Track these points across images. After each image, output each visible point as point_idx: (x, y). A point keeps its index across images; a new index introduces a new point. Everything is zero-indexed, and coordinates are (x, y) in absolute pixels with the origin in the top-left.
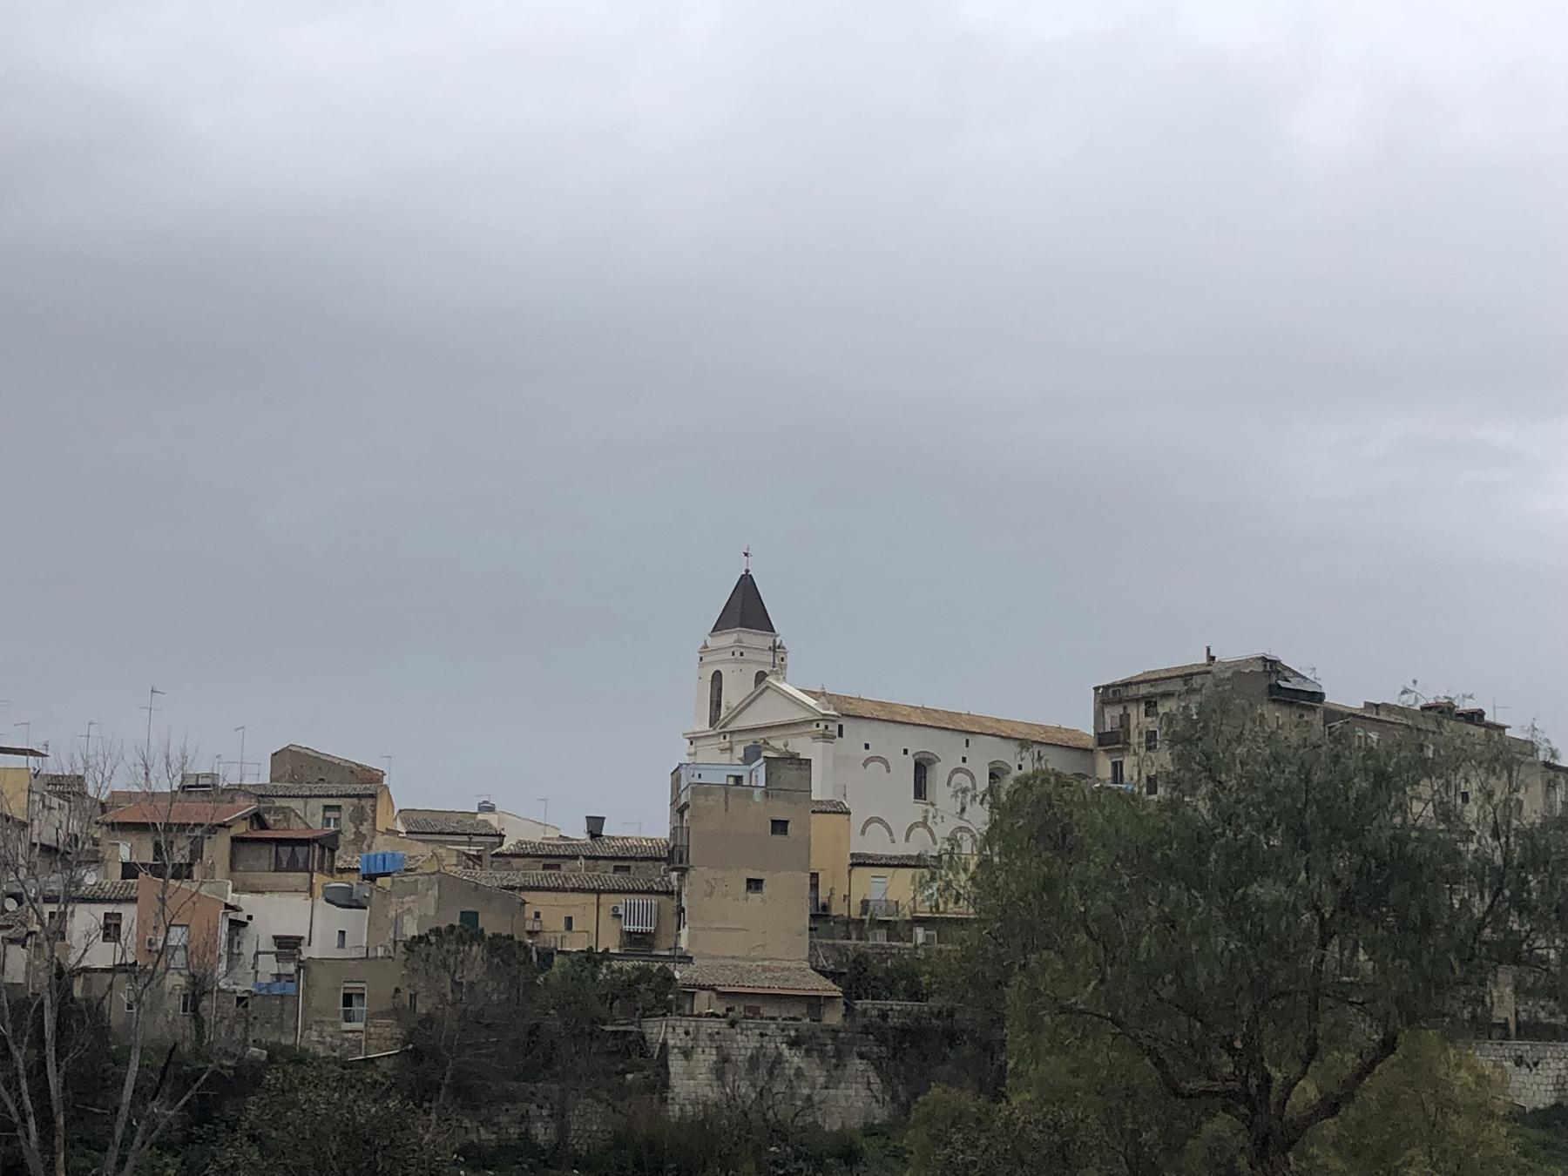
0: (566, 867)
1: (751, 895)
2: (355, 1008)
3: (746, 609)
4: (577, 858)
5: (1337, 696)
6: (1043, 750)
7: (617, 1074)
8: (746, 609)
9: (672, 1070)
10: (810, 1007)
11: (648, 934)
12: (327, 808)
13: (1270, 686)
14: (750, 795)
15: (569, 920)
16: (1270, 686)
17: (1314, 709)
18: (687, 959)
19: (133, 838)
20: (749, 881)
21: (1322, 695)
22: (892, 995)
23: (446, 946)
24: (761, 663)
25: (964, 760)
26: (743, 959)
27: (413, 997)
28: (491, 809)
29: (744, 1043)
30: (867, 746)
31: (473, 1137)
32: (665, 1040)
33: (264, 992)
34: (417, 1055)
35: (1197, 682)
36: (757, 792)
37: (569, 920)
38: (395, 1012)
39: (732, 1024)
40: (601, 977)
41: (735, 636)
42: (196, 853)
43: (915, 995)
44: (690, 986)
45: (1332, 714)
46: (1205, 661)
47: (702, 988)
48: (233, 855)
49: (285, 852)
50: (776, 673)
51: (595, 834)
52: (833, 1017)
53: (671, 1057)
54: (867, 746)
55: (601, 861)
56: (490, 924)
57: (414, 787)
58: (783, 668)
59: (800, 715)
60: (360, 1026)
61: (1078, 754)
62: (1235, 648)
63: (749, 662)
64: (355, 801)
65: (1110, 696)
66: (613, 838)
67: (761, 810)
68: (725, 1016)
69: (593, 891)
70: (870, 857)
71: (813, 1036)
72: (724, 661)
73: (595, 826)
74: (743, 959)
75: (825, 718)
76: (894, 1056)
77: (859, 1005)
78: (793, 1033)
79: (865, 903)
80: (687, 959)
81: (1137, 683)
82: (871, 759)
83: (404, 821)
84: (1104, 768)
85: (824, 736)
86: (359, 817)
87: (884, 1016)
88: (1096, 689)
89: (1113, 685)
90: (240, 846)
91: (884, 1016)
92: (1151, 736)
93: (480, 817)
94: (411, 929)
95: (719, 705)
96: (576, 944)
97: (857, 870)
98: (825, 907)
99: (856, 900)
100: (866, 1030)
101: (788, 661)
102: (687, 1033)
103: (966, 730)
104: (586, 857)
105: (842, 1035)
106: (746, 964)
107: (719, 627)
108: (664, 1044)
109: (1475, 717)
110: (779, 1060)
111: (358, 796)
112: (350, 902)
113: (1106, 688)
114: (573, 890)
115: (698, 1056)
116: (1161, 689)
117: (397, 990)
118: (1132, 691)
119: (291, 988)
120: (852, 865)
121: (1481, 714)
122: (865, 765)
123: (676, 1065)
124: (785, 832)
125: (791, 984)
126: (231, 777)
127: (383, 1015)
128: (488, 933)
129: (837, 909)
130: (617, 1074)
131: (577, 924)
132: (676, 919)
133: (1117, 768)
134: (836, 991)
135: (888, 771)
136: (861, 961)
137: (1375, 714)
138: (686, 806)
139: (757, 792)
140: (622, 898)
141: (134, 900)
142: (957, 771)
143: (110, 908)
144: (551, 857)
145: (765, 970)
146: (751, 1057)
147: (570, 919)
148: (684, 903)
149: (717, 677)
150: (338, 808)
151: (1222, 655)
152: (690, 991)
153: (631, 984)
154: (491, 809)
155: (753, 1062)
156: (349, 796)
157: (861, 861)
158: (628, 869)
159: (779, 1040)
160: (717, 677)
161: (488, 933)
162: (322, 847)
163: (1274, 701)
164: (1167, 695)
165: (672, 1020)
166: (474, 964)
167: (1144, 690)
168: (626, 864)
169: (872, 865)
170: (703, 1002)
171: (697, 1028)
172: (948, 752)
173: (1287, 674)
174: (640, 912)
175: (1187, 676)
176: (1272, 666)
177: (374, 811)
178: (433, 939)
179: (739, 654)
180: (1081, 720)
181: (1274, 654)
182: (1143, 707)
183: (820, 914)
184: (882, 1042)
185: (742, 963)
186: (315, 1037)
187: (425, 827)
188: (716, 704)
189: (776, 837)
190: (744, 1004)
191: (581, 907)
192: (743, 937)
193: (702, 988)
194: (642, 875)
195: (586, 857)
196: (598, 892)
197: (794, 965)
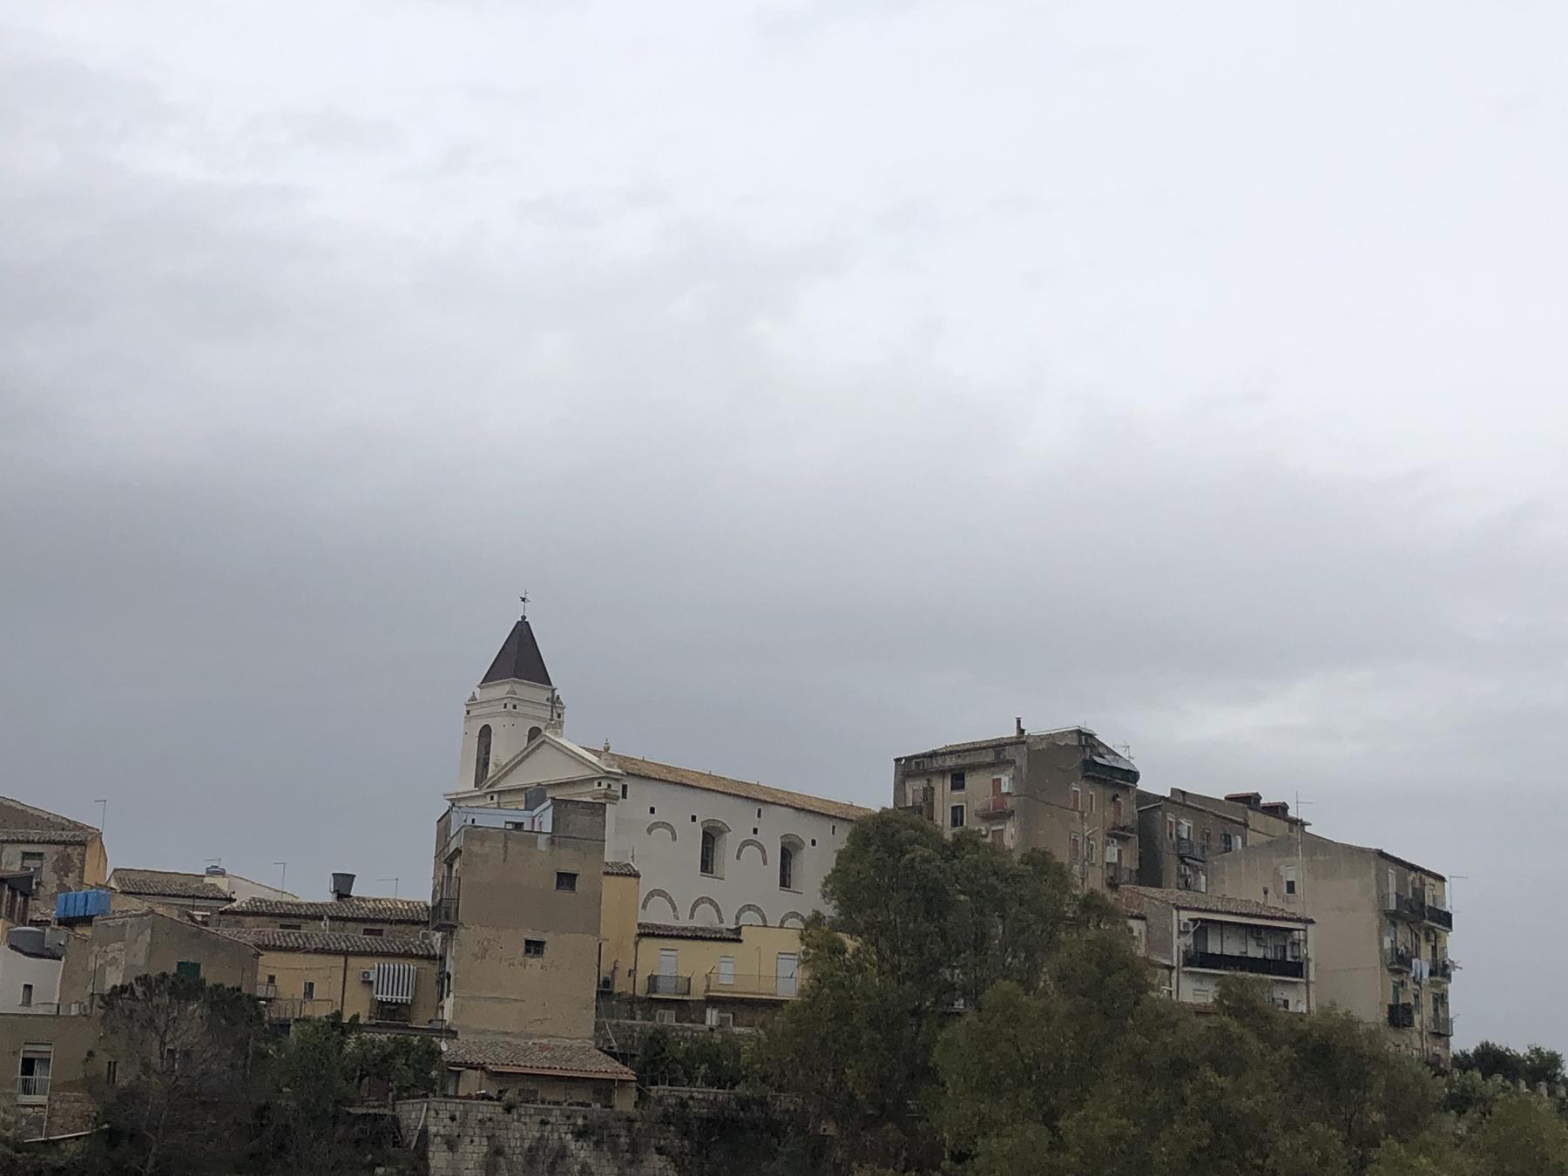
2: (38, 1075)
3: (521, 658)
4: (321, 918)
7: (365, 1167)
8: (521, 658)
9: (432, 1163)
10: (597, 1092)
13: (1085, 761)
14: (533, 843)
16: (1085, 761)
17: (1126, 788)
18: (451, 1034)
20: (528, 942)
21: (1133, 776)
22: (691, 1080)
23: (156, 1001)
24: (534, 718)
25: (755, 831)
26: (516, 1036)
27: (112, 1066)
28: (222, 873)
29: (521, 1133)
30: (652, 810)
32: (425, 1128)
34: (113, 1137)
36: (542, 840)
38: (89, 1084)
39: (508, 1109)
40: (348, 1049)
41: (507, 688)
43: (715, 1081)
44: (456, 1064)
45: (1144, 797)
46: (1014, 734)
47: (471, 1067)
50: (554, 727)
51: (342, 893)
52: (625, 1103)
53: (432, 1148)
54: (652, 810)
55: (352, 924)
56: (210, 976)
57: (128, 849)
58: (561, 724)
59: (588, 773)
62: (1048, 718)
63: (526, 716)
64: (61, 848)
65: (911, 768)
66: (363, 900)
67: (544, 861)
68: (499, 1099)
69: (337, 953)
70: (658, 927)
71: (603, 1126)
72: (499, 714)
73: (343, 884)
74: (516, 1036)
75: (609, 776)
76: (699, 1152)
77: (656, 1091)
78: (580, 1122)
79: (653, 980)
80: (451, 1034)
81: (943, 754)
83: (120, 880)
87: (683, 1104)
88: (898, 760)
89: (916, 757)
91: (683, 1104)
93: (207, 880)
94: (114, 979)
95: (486, 765)
96: (321, 1011)
97: (645, 941)
98: (607, 983)
99: (642, 976)
100: (667, 1119)
101: (565, 717)
102: (453, 1119)
103: (758, 799)
104: (331, 918)
105: (637, 1125)
106: (521, 1042)
107: (492, 676)
108: (424, 1132)
109: (1278, 810)
110: (562, 1154)
111: (64, 843)
112: (40, 952)
113: (909, 759)
114: (316, 951)
115: (465, 1147)
116: (968, 761)
117: (90, 1054)
118: (938, 763)
120: (641, 935)
121: (1284, 807)
122: (649, 831)
124: (572, 887)
125: (575, 1065)
127: (69, 1085)
128: (209, 984)
129: (621, 986)
130: (365, 1167)
132: (436, 990)
134: (628, 1073)
135: (674, 838)
136: (657, 1041)
137: (1181, 801)
138: (458, 851)
139: (542, 840)
140: (375, 963)
144: (291, 916)
145: (543, 1048)
146: (530, 1149)
147: (311, 985)
148: (450, 967)
149: (486, 732)
150: (40, 855)
151: (1031, 729)
152: (454, 1071)
153: (386, 1058)
154: (222, 873)
155: (531, 1155)
156: (54, 843)
157: (649, 933)
158: (380, 932)
159: (563, 1129)
160: (486, 732)
161: (209, 984)
162: (10, 888)
163: (1088, 778)
164: (974, 768)
165: (434, 1102)
166: (191, 1024)
167: (950, 762)
168: (378, 927)
169: (659, 936)
170: (471, 1083)
171: (466, 1114)
172: (738, 821)
173: (1101, 750)
174: (394, 980)
175: (998, 746)
176: (1086, 740)
177: (83, 861)
178: (139, 990)
179: (512, 707)
181: (1090, 727)
182: (948, 782)
183: (605, 989)
184: (686, 1134)
185: (515, 1042)
187: (137, 885)
188: (483, 763)
189: (560, 892)
190: (517, 1086)
192: (515, 1008)
193: (471, 1067)
194: (396, 938)
195: (331, 918)
196: (346, 954)
197: (577, 1043)
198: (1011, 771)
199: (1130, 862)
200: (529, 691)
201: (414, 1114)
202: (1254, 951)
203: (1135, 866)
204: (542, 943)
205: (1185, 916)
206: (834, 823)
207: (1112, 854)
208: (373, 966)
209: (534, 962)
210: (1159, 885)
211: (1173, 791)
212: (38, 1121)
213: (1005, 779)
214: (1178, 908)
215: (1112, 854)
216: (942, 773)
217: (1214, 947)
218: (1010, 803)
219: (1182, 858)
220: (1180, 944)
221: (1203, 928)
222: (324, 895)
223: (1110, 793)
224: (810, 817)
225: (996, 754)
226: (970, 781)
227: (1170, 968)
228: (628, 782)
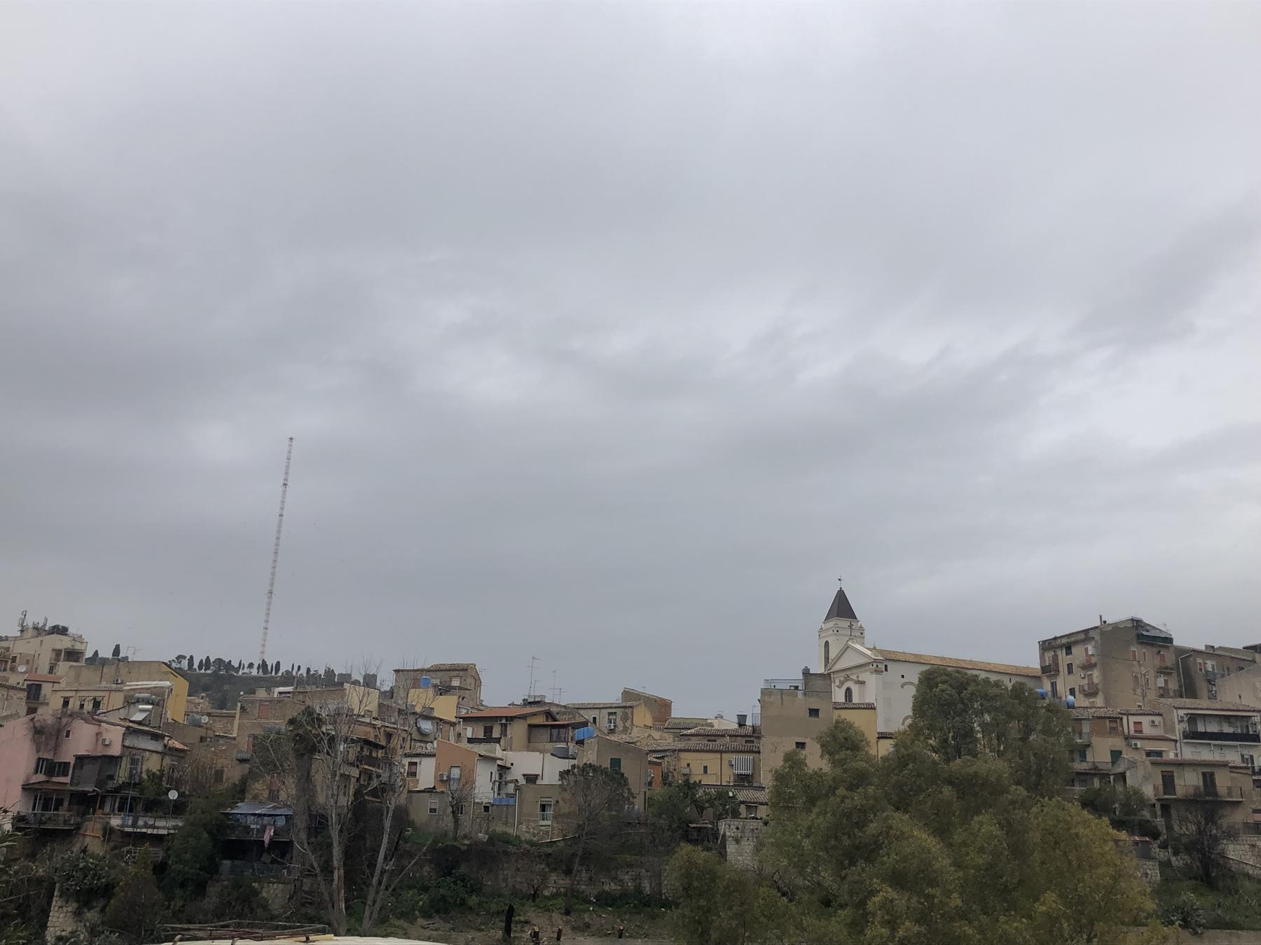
0: (720, 741)
3: (842, 608)
12: (610, 714)
15: (705, 768)
21: (1170, 640)
31: (606, 888)
35: (1091, 634)
37: (705, 768)
42: (504, 733)
45: (1181, 651)
47: (761, 804)
48: (530, 734)
49: (555, 731)
59: (867, 660)
60: (549, 823)
61: (278, 511)
62: (1116, 616)
65: (1046, 646)
75: (881, 662)
82: (906, 683)
84: (1047, 687)
86: (625, 719)
90: (535, 731)
92: (1070, 666)
97: (882, 741)
108: (724, 835)
119: (511, 801)
123: (731, 848)
126: (718, 726)
131: (711, 771)
133: (1054, 685)
139: (800, 694)
140: (734, 756)
149: (827, 643)
160: (827, 643)
164: (1076, 642)
167: (1064, 641)
171: (744, 826)
176: (1137, 624)
180: (1031, 660)
181: (1138, 616)
186: (524, 828)
188: (827, 658)
191: (712, 760)
193: (761, 804)
196: (721, 752)
198: (1093, 643)
199: (1173, 685)
200: (844, 623)
201: (727, 828)
202: (1228, 729)
203: (1177, 687)
205: (1181, 712)
207: (1161, 682)
210: (1195, 697)
211: (1207, 646)
212: (547, 833)
213: (1090, 647)
215: (1161, 682)
216: (1061, 647)
217: (1201, 728)
218: (1093, 660)
219: (1209, 681)
220: (1180, 728)
221: (1193, 719)
222: (733, 725)
223: (1155, 650)
225: (1085, 636)
226: (1074, 650)
227: (1176, 741)
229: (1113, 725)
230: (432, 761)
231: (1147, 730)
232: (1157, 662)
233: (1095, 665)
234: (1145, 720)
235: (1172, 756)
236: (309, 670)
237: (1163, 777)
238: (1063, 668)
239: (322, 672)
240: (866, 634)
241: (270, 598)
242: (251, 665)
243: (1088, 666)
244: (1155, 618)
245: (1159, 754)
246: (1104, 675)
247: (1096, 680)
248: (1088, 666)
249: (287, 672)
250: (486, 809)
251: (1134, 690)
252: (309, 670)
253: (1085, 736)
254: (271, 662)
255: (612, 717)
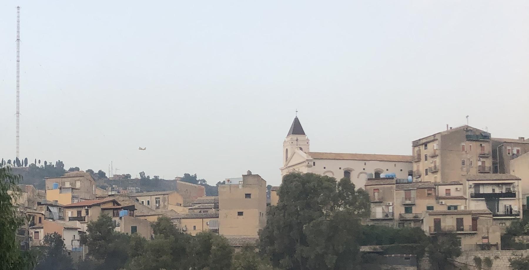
1: (239, 216)
3: (297, 129)
5: (495, 135)
6: (396, 163)
8: (297, 129)
11: (216, 230)
12: (156, 198)
15: (195, 227)
19: (72, 210)
25: (364, 169)
33: (74, 250)
37: (195, 227)
54: (325, 168)
65: (416, 144)
85: (307, 166)
86: (164, 201)
92: (426, 157)
111: (164, 195)
133: (418, 166)
141: (42, 228)
142: (361, 173)
143: (436, 217)
150: (159, 198)
167: (424, 141)
188: (287, 158)
189: (247, 199)
196: (203, 218)
199: (489, 163)
204: (242, 212)
205: (471, 183)
206: (395, 163)
208: (208, 220)
209: (241, 217)
214: (468, 180)
216: (422, 144)
224: (386, 162)
225: (433, 139)
228: (314, 161)
229: (430, 192)
230: (42, 230)
231: (453, 194)
232: (479, 151)
233: (437, 156)
234: (452, 188)
235: (462, 208)
236: (46, 163)
237: (435, 221)
238: (423, 158)
239: (54, 164)
240: (310, 142)
241: (18, 117)
242: (9, 162)
243: (434, 156)
244: (478, 124)
245: (456, 207)
246: (443, 162)
247: (437, 164)
248: (434, 156)
249: (32, 164)
250: (69, 253)
251: (462, 168)
252: (46, 163)
253: (412, 199)
254: (21, 159)
255: (158, 200)
